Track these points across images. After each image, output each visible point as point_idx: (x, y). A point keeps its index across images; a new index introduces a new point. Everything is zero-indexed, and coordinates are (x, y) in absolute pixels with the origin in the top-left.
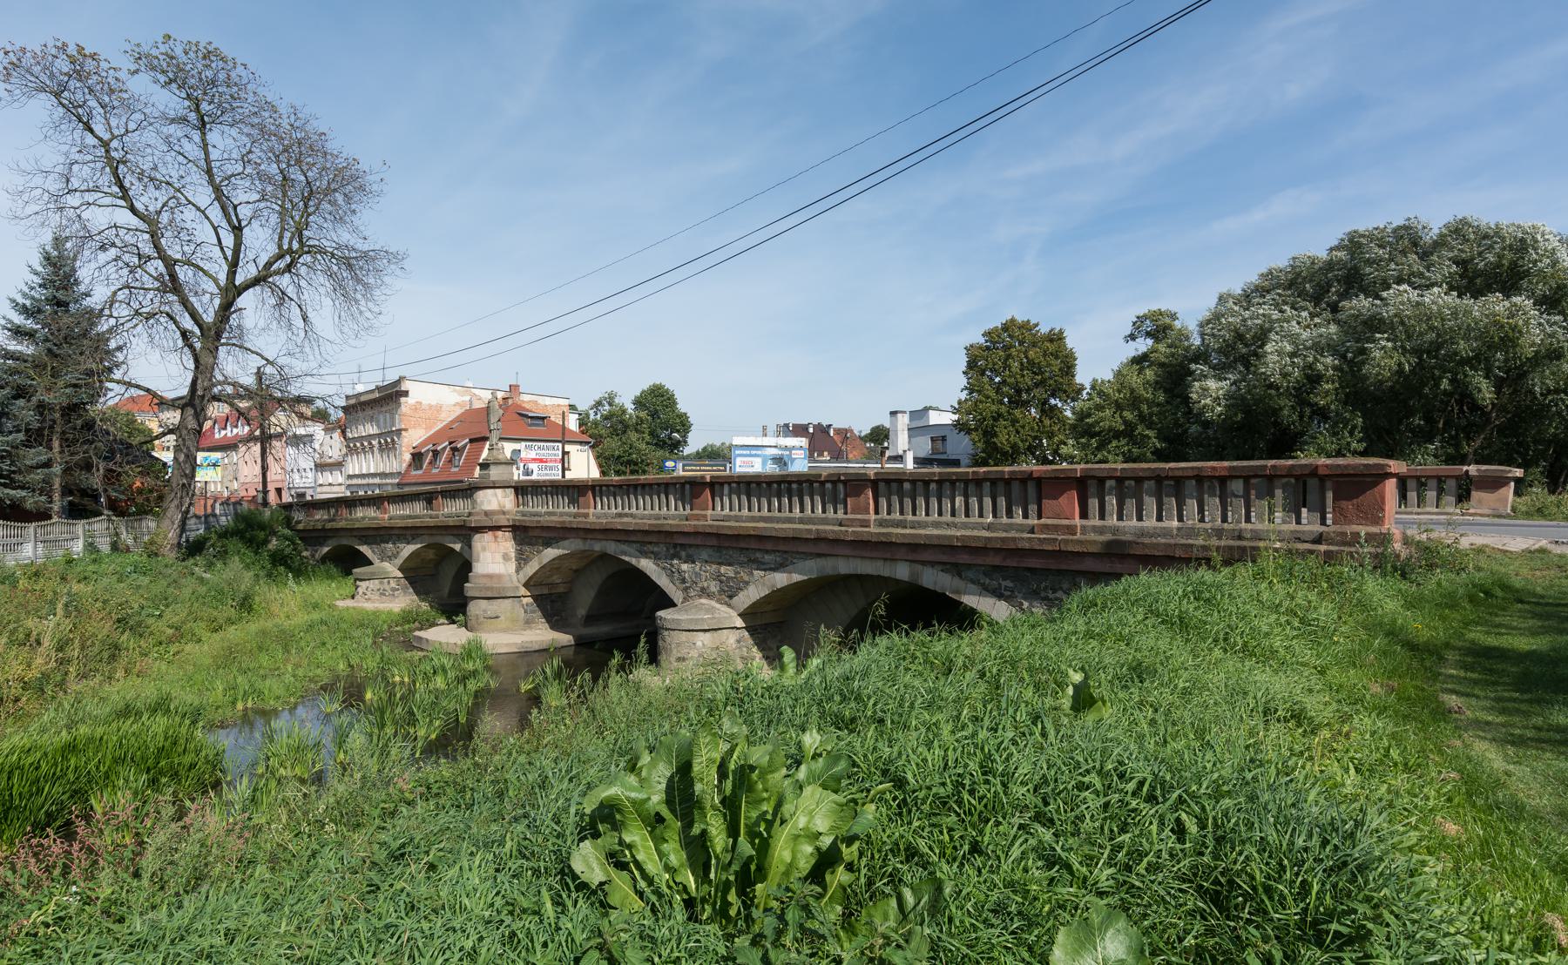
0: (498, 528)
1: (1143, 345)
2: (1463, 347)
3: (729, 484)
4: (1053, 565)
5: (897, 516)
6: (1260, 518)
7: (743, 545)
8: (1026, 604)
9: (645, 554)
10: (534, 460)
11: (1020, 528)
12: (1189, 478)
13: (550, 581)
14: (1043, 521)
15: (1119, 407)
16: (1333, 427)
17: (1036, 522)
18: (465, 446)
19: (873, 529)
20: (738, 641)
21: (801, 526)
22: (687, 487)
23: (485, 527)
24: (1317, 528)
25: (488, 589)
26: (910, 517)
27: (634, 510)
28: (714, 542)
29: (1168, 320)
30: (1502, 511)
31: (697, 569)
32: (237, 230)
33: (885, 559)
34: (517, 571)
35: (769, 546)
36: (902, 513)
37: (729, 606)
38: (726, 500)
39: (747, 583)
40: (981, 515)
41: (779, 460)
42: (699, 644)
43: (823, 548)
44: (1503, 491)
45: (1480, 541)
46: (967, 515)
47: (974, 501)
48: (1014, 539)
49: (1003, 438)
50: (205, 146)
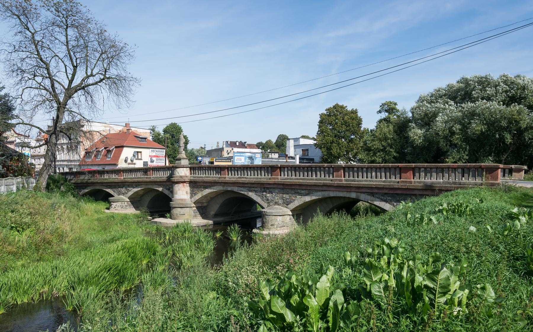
0: (184, 182)
1: (384, 115)
2: (504, 123)
3: (287, 168)
4: (404, 192)
5: (351, 178)
6: (465, 179)
7: (293, 188)
8: (395, 204)
9: (251, 191)
10: (155, 156)
11: (394, 182)
12: (446, 168)
13: (202, 202)
14: (402, 180)
15: (380, 140)
16: (458, 150)
17: (399, 180)
18: (113, 150)
19: (343, 182)
20: (290, 219)
21: (317, 181)
22: (270, 168)
23: (180, 182)
24: (481, 182)
25: (181, 204)
26: (356, 179)
27: (246, 176)
28: (282, 187)
29: (393, 106)
30: (521, 179)
31: (274, 196)
32: (75, 67)
33: (347, 192)
34: (191, 198)
35: (304, 188)
36: (353, 177)
37: (287, 208)
38: (286, 173)
39: (294, 200)
40: (381, 178)
41: (251, 158)
42: (278, 220)
43: (325, 188)
44: (521, 173)
45: (520, 185)
46: (376, 178)
47: (379, 174)
48: (393, 185)
49: (335, 150)
50: (67, 36)
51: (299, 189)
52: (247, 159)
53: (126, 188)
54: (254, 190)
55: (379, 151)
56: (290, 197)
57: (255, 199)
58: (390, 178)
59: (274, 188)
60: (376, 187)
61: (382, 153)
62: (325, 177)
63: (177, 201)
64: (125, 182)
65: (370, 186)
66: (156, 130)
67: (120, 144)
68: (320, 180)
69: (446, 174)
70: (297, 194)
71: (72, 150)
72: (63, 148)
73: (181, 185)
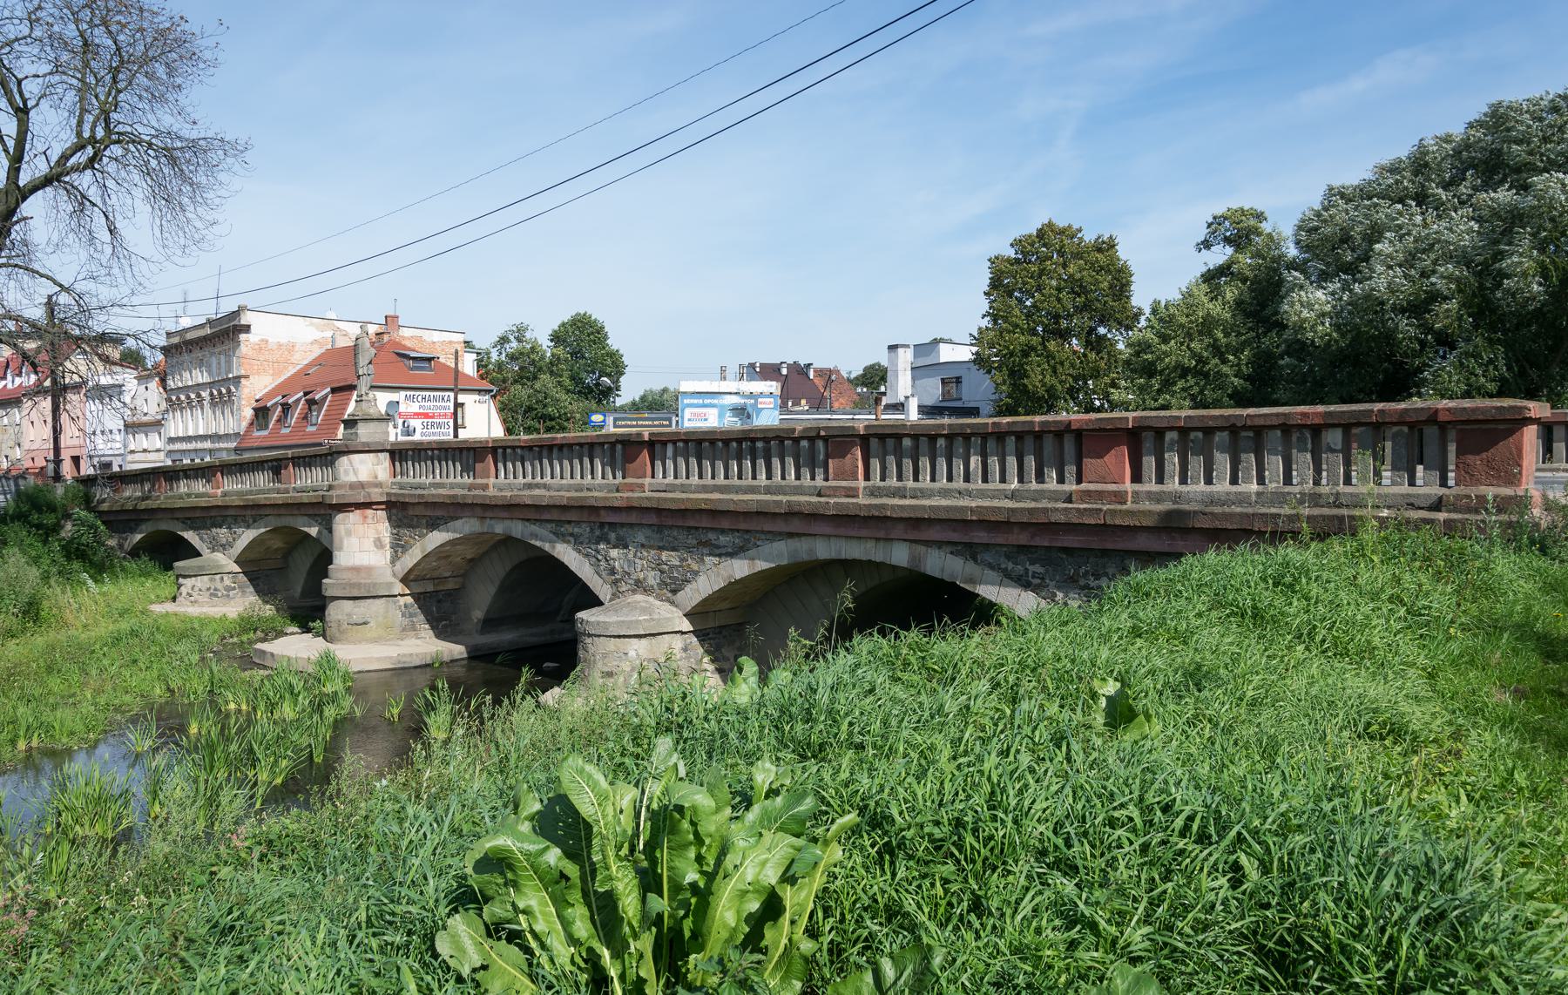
0: (367, 505)
1: (1220, 255)
3: (674, 443)
4: (1095, 543)
5: (893, 482)
7: (692, 523)
9: (562, 537)
10: (417, 415)
11: (1054, 495)
13: (436, 574)
14: (1084, 486)
17: (1074, 487)
18: (325, 397)
19: (862, 500)
20: (685, 649)
21: (768, 497)
22: (619, 447)
24: (1436, 491)
25: (353, 585)
26: (910, 484)
27: (548, 479)
28: (653, 519)
29: (1252, 222)
31: (631, 555)
33: (878, 539)
34: (393, 562)
35: (725, 524)
36: (900, 478)
37: (672, 603)
39: (696, 573)
40: (1003, 480)
41: (740, 411)
42: (632, 654)
43: (796, 525)
46: (985, 480)
47: (994, 462)
48: (1045, 510)
49: (1037, 378)
51: (712, 529)
52: (729, 414)
53: (229, 528)
54: (572, 535)
55: (1183, 376)
56: (683, 560)
57: (573, 569)
58: (1040, 477)
59: (631, 525)
60: (980, 522)
61: (1192, 382)
62: (798, 477)
63: (339, 575)
64: (226, 507)
65: (959, 517)
66: (528, 335)
67: (346, 380)
68: (779, 490)
69: (1273, 458)
70: (705, 551)
71: (182, 409)
72: (201, 400)
73: (354, 517)
